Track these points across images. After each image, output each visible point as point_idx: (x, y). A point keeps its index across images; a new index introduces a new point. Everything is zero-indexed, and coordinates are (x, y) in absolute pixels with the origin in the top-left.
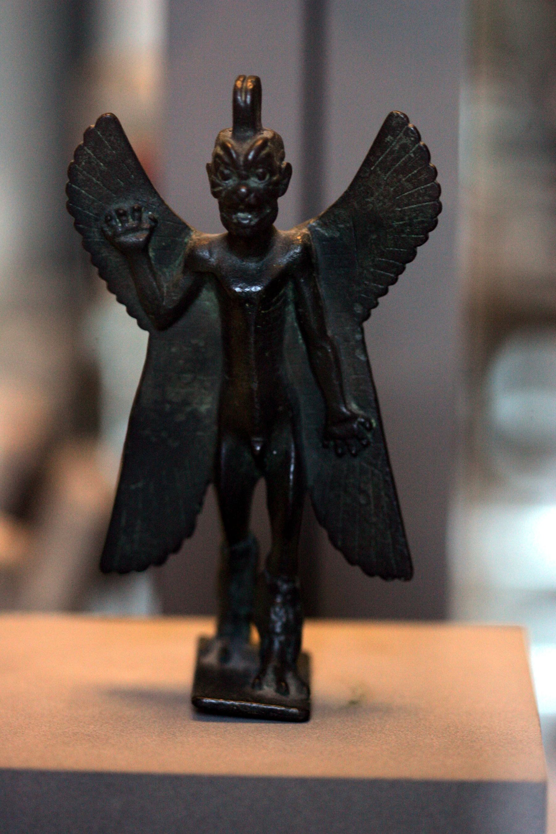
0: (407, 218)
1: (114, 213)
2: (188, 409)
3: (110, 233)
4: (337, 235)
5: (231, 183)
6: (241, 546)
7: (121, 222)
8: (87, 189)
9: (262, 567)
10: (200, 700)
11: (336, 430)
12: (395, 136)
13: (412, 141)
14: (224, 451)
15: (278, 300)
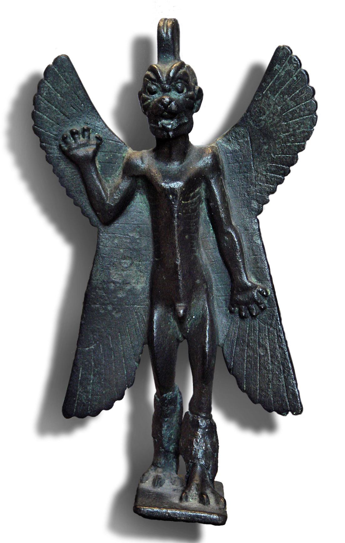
0: (291, 130)
2: (128, 287)
3: (66, 148)
4: (237, 148)
5: (157, 96)
6: (169, 395)
8: (47, 114)
9: (186, 409)
11: (240, 297)
12: (281, 65)
13: (295, 67)
15: (194, 197)
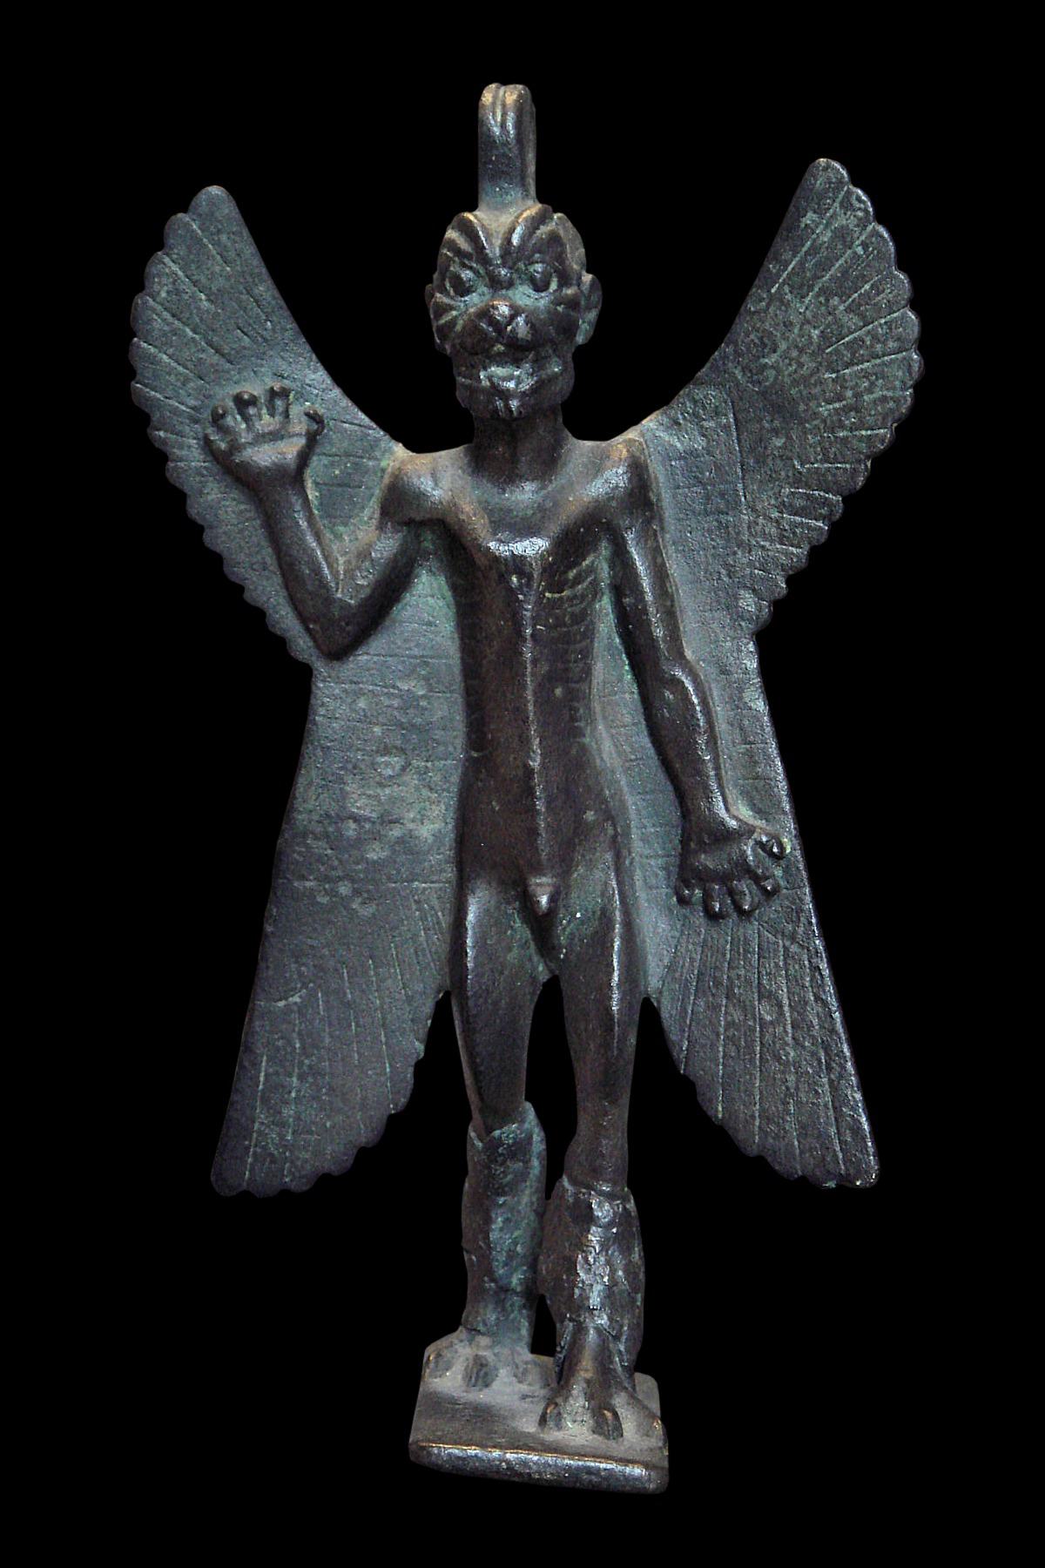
0: (849, 393)
1: (231, 404)
2: (396, 832)
3: (223, 446)
4: (700, 444)
7: (246, 419)
8: (171, 351)
10: (423, 1448)
11: (707, 861)
13: (860, 219)
14: (471, 917)
